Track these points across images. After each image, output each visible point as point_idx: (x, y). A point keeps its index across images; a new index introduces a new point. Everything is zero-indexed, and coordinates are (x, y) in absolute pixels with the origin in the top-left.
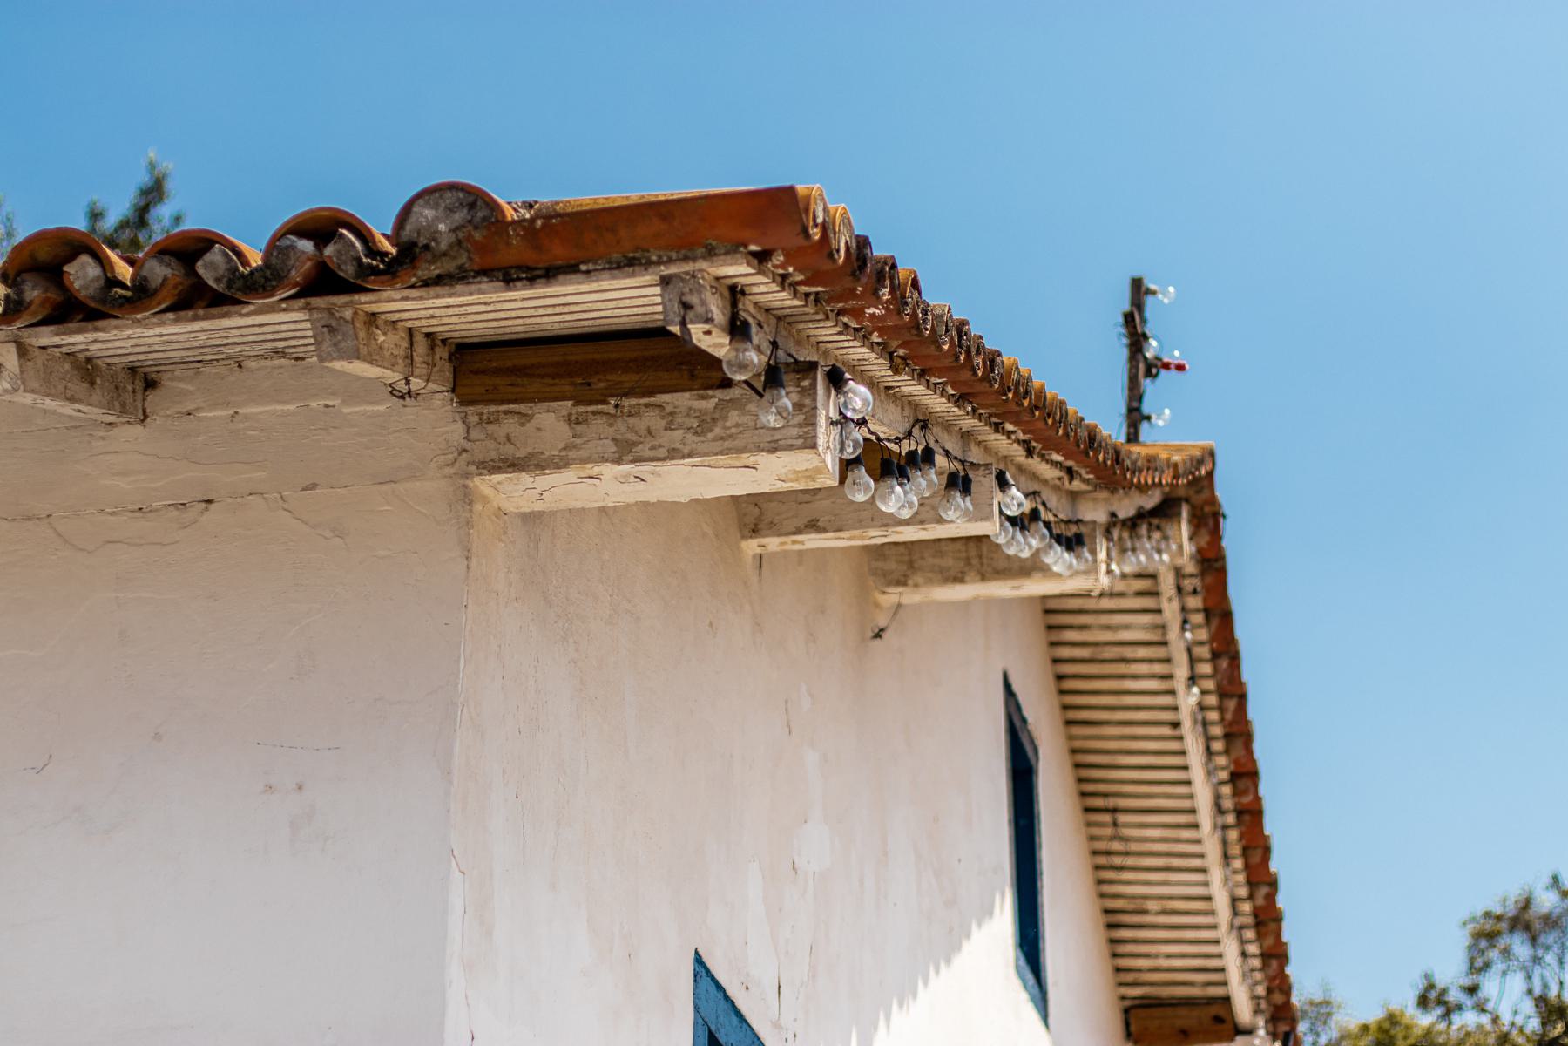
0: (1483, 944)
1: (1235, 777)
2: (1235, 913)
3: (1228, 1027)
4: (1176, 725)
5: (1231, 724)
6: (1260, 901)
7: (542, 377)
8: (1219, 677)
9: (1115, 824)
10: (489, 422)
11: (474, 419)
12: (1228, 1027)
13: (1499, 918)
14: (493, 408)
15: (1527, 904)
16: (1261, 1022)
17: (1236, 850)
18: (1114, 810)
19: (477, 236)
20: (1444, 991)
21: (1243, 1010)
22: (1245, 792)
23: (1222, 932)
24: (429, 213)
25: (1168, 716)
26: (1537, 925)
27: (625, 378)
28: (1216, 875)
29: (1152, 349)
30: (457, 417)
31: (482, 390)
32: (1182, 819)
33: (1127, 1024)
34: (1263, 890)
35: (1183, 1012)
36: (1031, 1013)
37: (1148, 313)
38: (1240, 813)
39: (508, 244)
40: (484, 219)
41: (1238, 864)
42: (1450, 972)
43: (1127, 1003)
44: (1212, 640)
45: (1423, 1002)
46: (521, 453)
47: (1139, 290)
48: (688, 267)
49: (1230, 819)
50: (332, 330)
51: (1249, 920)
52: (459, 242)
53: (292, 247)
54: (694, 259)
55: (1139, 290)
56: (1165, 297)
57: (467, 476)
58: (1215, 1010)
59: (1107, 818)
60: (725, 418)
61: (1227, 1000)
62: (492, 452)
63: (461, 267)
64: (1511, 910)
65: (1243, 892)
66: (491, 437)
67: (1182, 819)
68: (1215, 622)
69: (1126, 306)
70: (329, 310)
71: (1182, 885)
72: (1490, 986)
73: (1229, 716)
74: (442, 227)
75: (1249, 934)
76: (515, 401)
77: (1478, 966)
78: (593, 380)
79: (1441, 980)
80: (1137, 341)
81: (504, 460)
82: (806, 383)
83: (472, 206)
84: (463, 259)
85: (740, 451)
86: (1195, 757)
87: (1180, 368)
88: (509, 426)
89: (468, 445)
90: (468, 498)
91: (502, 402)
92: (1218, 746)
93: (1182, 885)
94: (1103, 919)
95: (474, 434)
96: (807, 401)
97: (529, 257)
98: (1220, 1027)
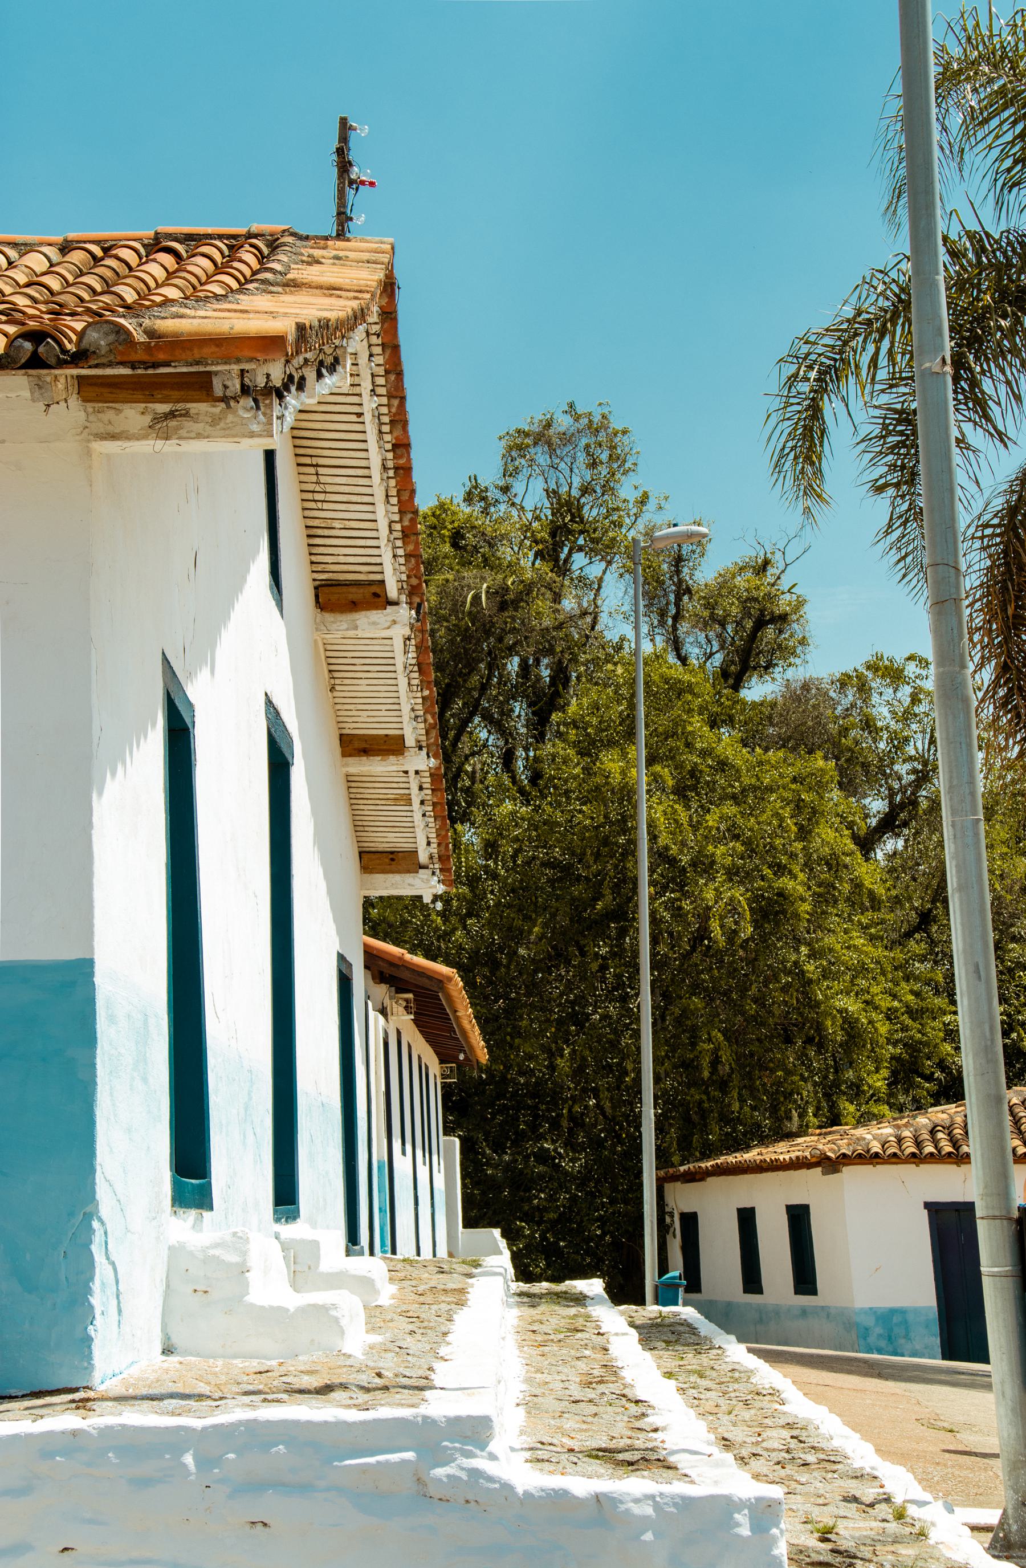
0: (514, 454)
1: (395, 447)
2: (391, 531)
3: (382, 600)
4: (360, 415)
5: (395, 415)
6: (406, 523)
7: (127, 389)
8: (389, 386)
9: (317, 474)
10: (99, 412)
11: (90, 410)
12: (382, 600)
13: (527, 435)
14: (100, 405)
15: (549, 425)
16: (403, 598)
17: (393, 492)
18: (317, 465)
19: (120, 348)
20: (487, 489)
21: (392, 590)
22: (401, 457)
23: (383, 542)
24: (95, 335)
25: (356, 409)
26: (556, 440)
27: (172, 393)
28: (381, 509)
29: (355, 173)
30: (82, 408)
31: (94, 395)
32: (360, 472)
33: (317, 596)
34: (409, 516)
35: (353, 590)
36: (278, 613)
37: (351, 144)
38: (396, 468)
39: (136, 353)
40: (124, 340)
41: (394, 500)
42: (490, 477)
43: (318, 583)
44: (386, 363)
45: (469, 498)
46: (117, 431)
47: (345, 127)
48: (227, 367)
49: (391, 473)
50: (40, 387)
51: (399, 535)
52: (111, 351)
53: (21, 347)
54: (230, 364)
55: (345, 127)
56: (361, 132)
57: (89, 441)
58: (374, 589)
59: (312, 470)
60: (226, 418)
61: (382, 582)
62: (100, 428)
63: (110, 361)
64: (536, 428)
65: (397, 518)
66: (100, 420)
67: (360, 472)
68: (388, 352)
69: (335, 144)
70: (39, 377)
71: (358, 512)
72: (518, 487)
73: (394, 410)
74: (102, 343)
75: (399, 543)
76: (112, 402)
77: (510, 472)
78: (155, 393)
79: (483, 483)
80: (344, 166)
81: (108, 434)
82: (267, 402)
83: (118, 332)
84: (112, 358)
85: (234, 436)
86: (372, 436)
87: (372, 184)
88: (110, 415)
89: (88, 424)
90: (89, 453)
91: (106, 402)
92: (386, 428)
93: (358, 512)
94: (305, 532)
95: (91, 418)
96: (268, 411)
97: (145, 357)
98: (377, 600)
